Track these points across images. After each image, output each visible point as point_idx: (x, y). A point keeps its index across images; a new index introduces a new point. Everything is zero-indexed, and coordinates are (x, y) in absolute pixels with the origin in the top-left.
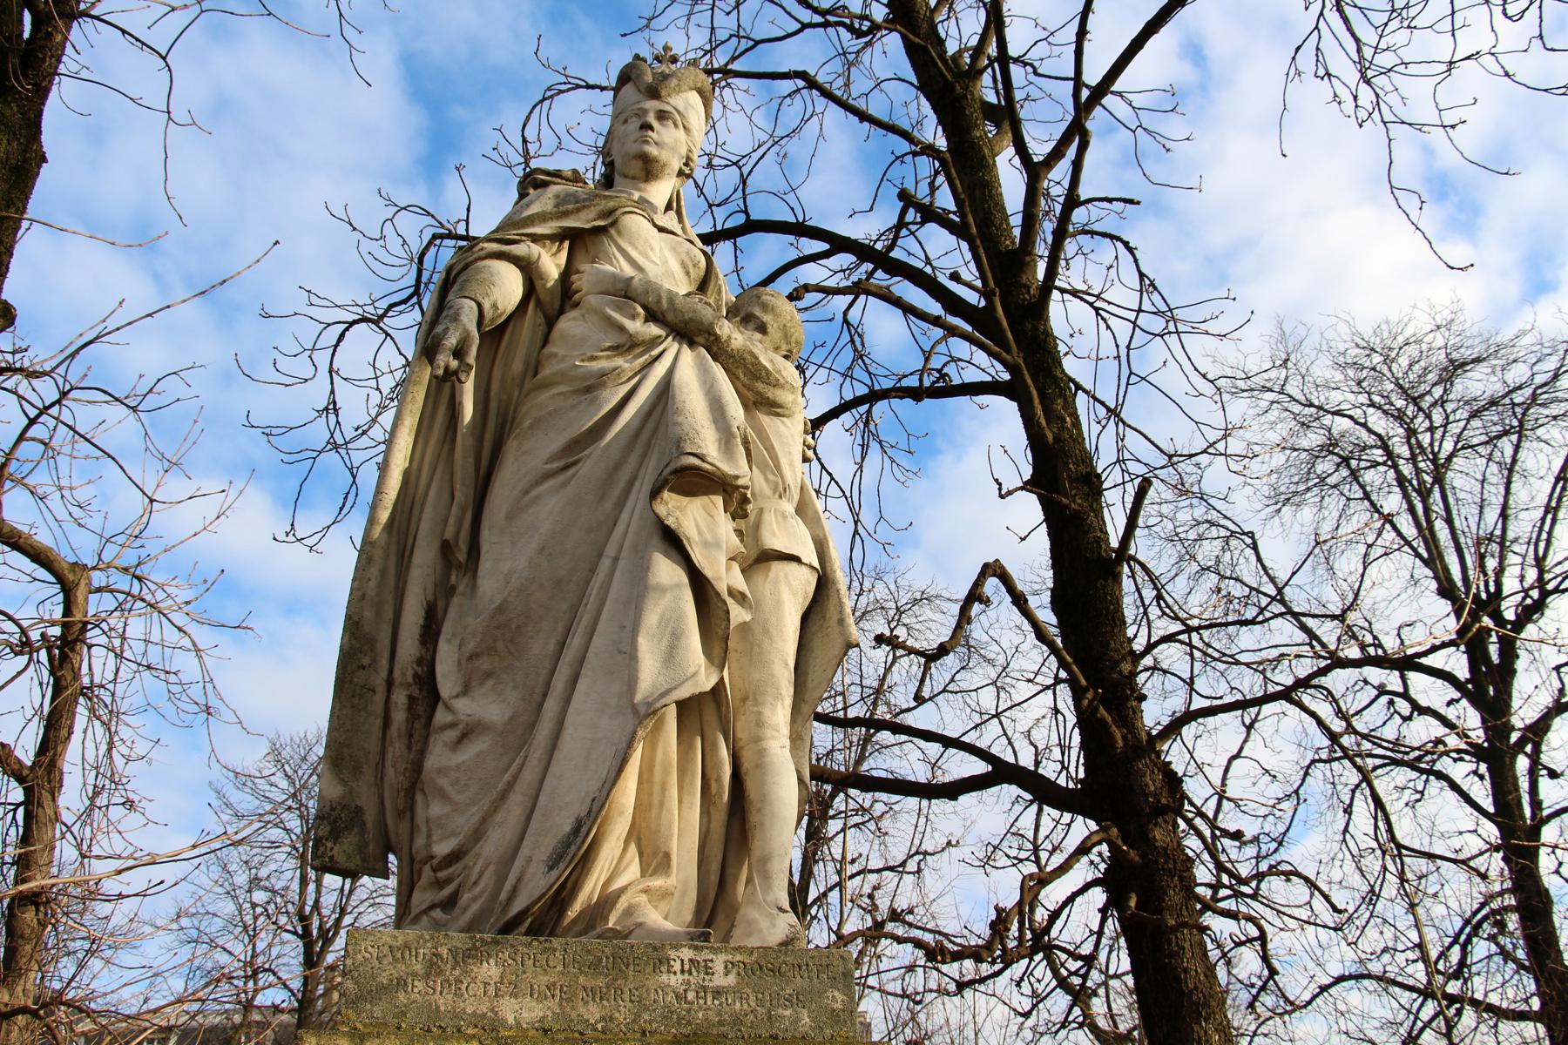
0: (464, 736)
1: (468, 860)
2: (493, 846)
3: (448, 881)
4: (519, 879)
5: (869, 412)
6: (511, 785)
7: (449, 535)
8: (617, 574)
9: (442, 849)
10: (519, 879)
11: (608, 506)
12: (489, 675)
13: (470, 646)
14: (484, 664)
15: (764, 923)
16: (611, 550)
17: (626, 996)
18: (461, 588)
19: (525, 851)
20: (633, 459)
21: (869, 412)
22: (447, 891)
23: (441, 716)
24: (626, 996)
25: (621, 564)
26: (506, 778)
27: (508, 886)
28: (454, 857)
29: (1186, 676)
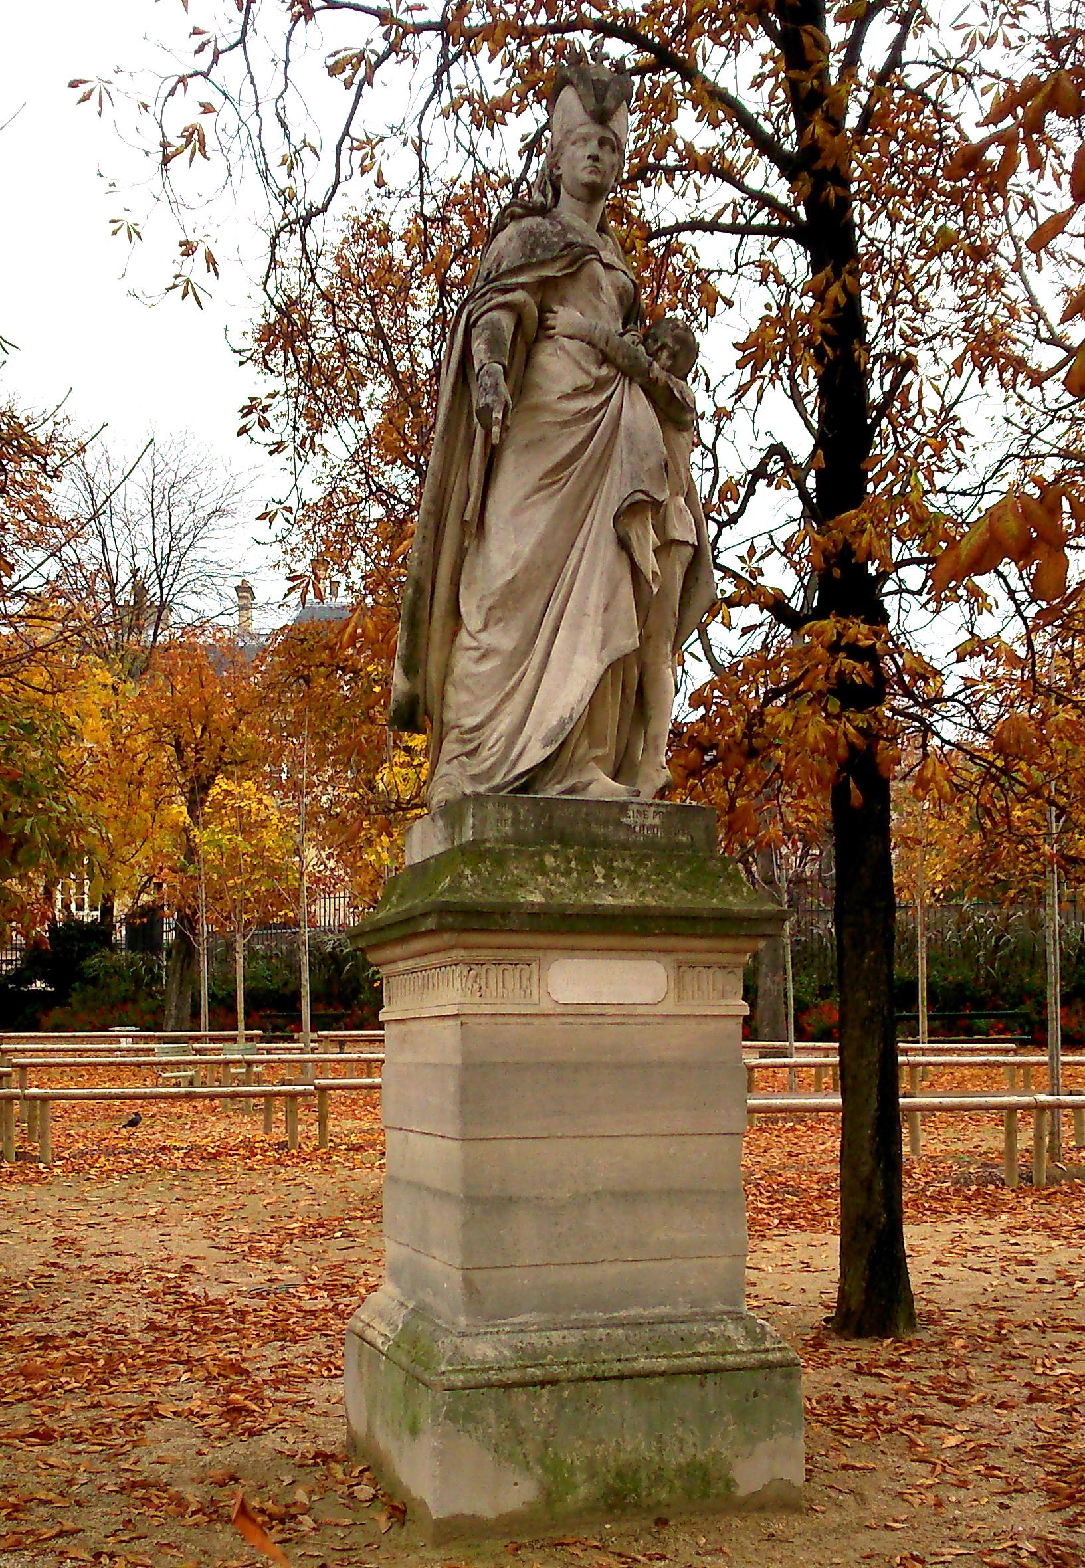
0: (484, 657)
1: (487, 730)
2: (503, 724)
3: (471, 741)
4: (524, 749)
5: (608, 381)
6: (514, 689)
7: (467, 518)
8: (584, 562)
9: (471, 722)
10: (524, 749)
11: (580, 514)
12: (500, 620)
13: (489, 602)
14: (498, 613)
15: (655, 775)
16: (579, 544)
17: (383, 468)
18: (471, 550)
19: (527, 730)
20: (597, 479)
21: (608, 381)
22: (471, 747)
23: (464, 639)
24: (383, 468)
25: (586, 555)
26: (511, 683)
27: (515, 752)
28: (478, 728)
29: (239, 50)
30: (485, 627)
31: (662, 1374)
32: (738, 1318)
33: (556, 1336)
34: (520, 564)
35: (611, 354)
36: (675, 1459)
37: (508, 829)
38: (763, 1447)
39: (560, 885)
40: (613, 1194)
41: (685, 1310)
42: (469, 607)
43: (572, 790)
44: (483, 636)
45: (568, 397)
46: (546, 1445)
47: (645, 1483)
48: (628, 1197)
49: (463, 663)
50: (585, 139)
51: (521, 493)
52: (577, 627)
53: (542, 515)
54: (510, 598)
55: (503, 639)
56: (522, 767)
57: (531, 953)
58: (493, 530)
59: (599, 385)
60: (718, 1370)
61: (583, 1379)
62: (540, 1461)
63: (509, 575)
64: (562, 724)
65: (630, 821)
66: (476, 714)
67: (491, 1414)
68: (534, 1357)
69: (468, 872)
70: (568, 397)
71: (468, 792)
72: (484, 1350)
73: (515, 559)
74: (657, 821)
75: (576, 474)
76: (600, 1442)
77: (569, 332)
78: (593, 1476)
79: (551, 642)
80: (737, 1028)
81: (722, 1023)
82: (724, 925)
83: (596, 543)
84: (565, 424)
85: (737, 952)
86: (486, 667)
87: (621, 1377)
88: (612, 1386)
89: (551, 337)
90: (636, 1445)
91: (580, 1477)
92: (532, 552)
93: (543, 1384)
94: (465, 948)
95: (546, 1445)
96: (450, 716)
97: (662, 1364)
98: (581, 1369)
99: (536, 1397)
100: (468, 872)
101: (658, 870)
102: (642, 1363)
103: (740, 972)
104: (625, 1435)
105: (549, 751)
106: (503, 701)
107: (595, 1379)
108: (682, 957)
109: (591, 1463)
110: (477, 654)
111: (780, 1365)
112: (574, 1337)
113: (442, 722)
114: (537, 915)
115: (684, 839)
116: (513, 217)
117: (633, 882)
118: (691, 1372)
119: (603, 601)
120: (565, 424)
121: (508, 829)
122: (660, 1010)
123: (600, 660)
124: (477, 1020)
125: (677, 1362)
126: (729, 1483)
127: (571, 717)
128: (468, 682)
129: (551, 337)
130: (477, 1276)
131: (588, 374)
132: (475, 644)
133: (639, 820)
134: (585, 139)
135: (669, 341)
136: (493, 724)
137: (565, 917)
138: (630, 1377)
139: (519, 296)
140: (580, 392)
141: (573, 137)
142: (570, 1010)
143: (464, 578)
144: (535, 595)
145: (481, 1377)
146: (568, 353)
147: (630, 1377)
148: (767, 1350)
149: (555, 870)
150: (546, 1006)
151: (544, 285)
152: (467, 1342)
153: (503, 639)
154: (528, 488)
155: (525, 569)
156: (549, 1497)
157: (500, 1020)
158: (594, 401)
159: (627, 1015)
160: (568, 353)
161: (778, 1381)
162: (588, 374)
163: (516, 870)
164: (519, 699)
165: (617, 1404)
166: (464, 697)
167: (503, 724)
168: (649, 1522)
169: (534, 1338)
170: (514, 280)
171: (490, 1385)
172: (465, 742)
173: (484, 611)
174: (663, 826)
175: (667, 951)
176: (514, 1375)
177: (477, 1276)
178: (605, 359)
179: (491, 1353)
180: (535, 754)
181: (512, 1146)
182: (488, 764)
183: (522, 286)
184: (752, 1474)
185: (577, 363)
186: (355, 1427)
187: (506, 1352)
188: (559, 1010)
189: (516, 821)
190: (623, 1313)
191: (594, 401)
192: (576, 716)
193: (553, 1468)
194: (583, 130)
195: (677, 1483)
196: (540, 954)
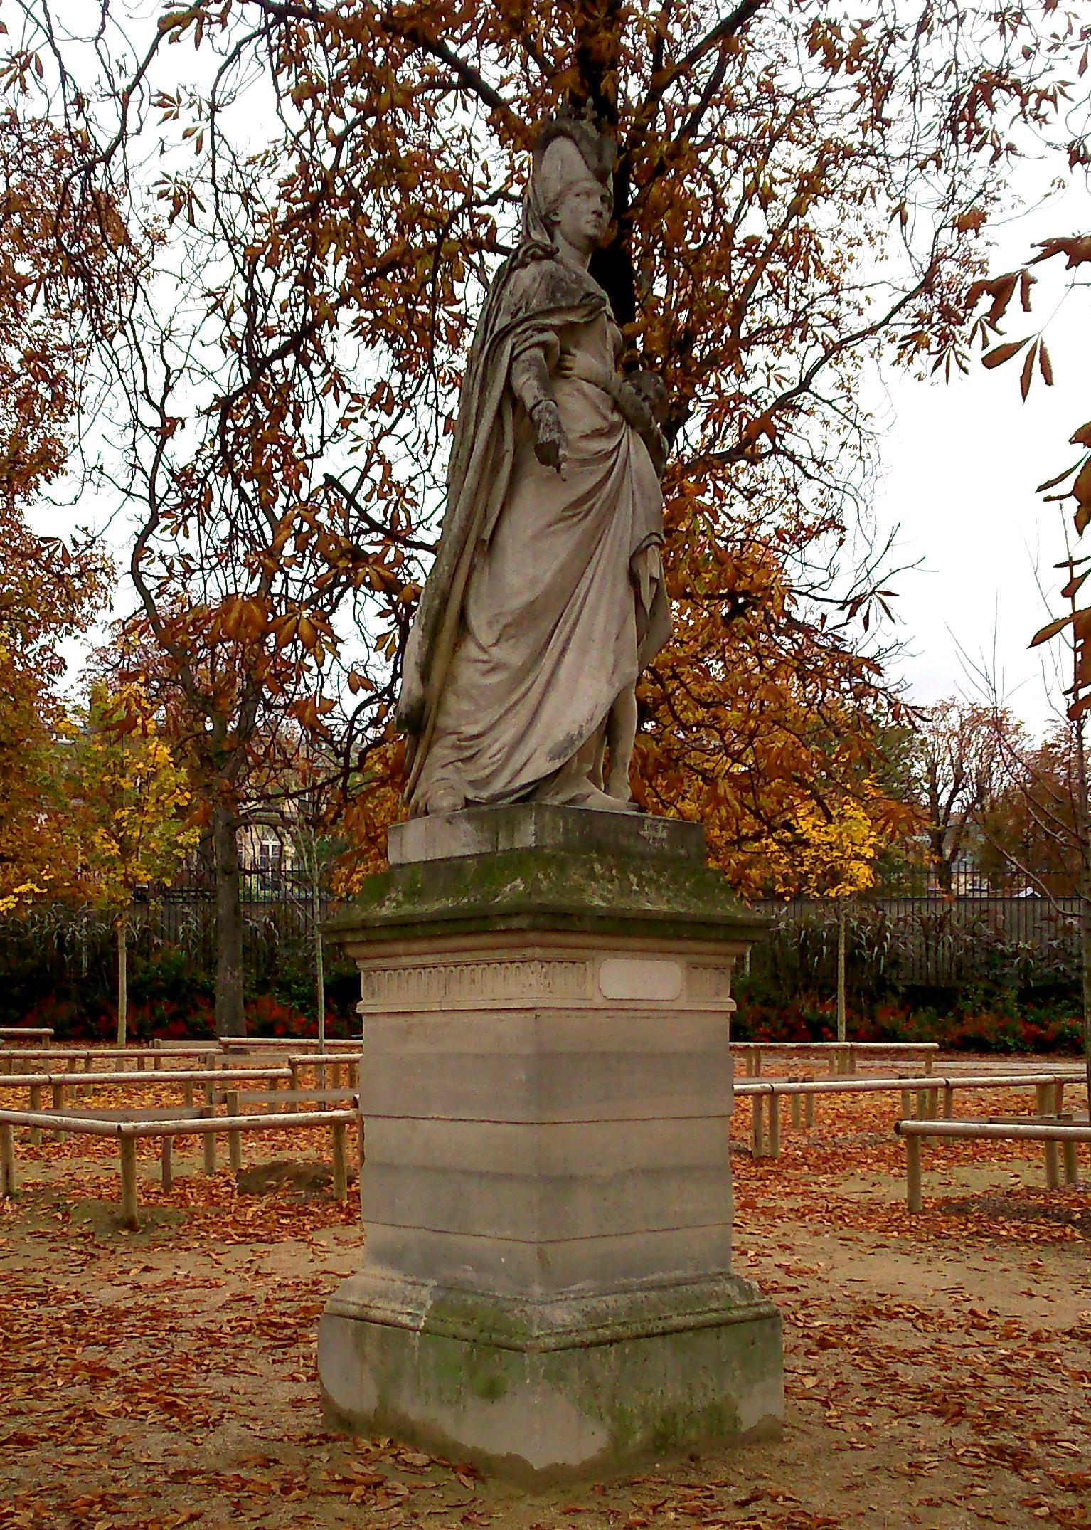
0: (493, 670)
1: (486, 740)
9: (473, 730)
13: (504, 621)
14: (511, 631)
16: (589, 574)
22: (467, 753)
23: (471, 650)
26: (515, 697)
28: (479, 736)
30: (495, 644)
31: (691, 1329)
32: (730, 1278)
33: (610, 1300)
34: (540, 587)
35: (622, 402)
36: (700, 1402)
37: (560, 838)
38: (758, 1388)
39: (610, 891)
40: (643, 1171)
41: (690, 1273)
42: (477, 620)
43: (570, 801)
44: (494, 650)
45: (585, 437)
46: (614, 1397)
47: (681, 1425)
48: (654, 1173)
49: (468, 674)
50: (588, 194)
51: (543, 522)
52: (584, 651)
53: (562, 546)
54: (528, 615)
55: (513, 655)
56: (527, 777)
57: (586, 952)
58: (510, 551)
59: (612, 430)
60: (729, 1323)
61: (638, 1337)
62: (610, 1412)
63: (527, 597)
64: (570, 740)
65: (645, 833)
66: (476, 722)
67: (574, 1372)
68: (596, 1319)
69: (541, 876)
70: (585, 437)
71: (470, 797)
72: (562, 1315)
73: (533, 581)
74: (664, 835)
75: (588, 511)
76: (651, 1391)
77: (588, 376)
78: (646, 1422)
79: (558, 662)
80: (725, 1022)
81: (716, 1018)
82: (727, 930)
83: (603, 578)
84: (584, 462)
85: (727, 955)
86: (493, 680)
87: (664, 1334)
88: (658, 1341)
89: (566, 377)
90: (674, 1394)
91: (638, 1423)
92: (554, 577)
93: (611, 1342)
94: (541, 946)
95: (614, 1397)
96: (447, 722)
97: (691, 1320)
98: (636, 1328)
99: (607, 1354)
100: (541, 876)
101: (674, 880)
102: (677, 1321)
103: (728, 972)
104: (667, 1384)
105: (557, 764)
106: (506, 713)
107: (647, 1336)
108: (696, 958)
109: (644, 1410)
110: (487, 667)
111: (769, 1316)
112: (623, 1300)
113: (434, 728)
114: (603, 917)
115: (683, 852)
116: (535, 258)
117: (658, 889)
118: (711, 1326)
119: (613, 631)
120: (584, 462)
121: (560, 838)
122: (676, 1006)
123: (610, 683)
124: (550, 1013)
125: (700, 1318)
126: (736, 1421)
127: (580, 735)
128: (474, 692)
129: (566, 377)
130: (548, 1249)
131: (605, 418)
132: (485, 657)
133: (653, 833)
134: (588, 194)
135: (651, 394)
136: (493, 734)
137: (623, 919)
138: (670, 1333)
139: (550, 336)
140: (597, 434)
141: (577, 189)
142: (615, 1005)
143: (472, 592)
144: (544, 620)
145: (567, 1339)
146: (585, 396)
147: (670, 1333)
148: (757, 1305)
149: (602, 877)
150: (598, 1002)
151: (566, 330)
152: (547, 1310)
153: (513, 655)
154: (550, 517)
155: (546, 594)
156: (617, 1441)
157: (563, 1013)
158: (609, 445)
159: (655, 1011)
160: (585, 396)
161: (767, 1330)
162: (605, 418)
163: (575, 876)
164: (524, 712)
165: (663, 1357)
166: (466, 706)
167: (507, 734)
168: (685, 1460)
169: (594, 1302)
170: (548, 321)
171: (574, 1347)
172: (460, 748)
173: (500, 626)
174: (670, 840)
175: (680, 953)
176: (590, 1336)
177: (548, 1249)
178: (616, 407)
179: (568, 1318)
180: (541, 766)
181: (572, 1128)
182: (487, 771)
183: (552, 327)
184: (750, 1415)
185: (597, 408)
186: (1068, 1322)
187: (578, 1316)
188: (608, 1005)
189: (566, 831)
190: (651, 1278)
191: (609, 445)
192: (586, 734)
193: (620, 1417)
194: (588, 185)
195: (702, 1423)
196: (594, 953)
